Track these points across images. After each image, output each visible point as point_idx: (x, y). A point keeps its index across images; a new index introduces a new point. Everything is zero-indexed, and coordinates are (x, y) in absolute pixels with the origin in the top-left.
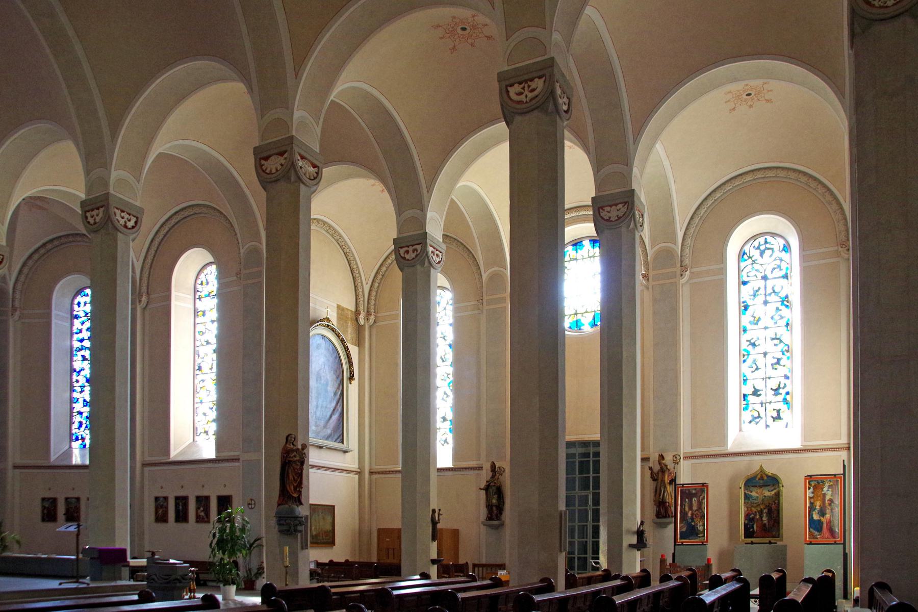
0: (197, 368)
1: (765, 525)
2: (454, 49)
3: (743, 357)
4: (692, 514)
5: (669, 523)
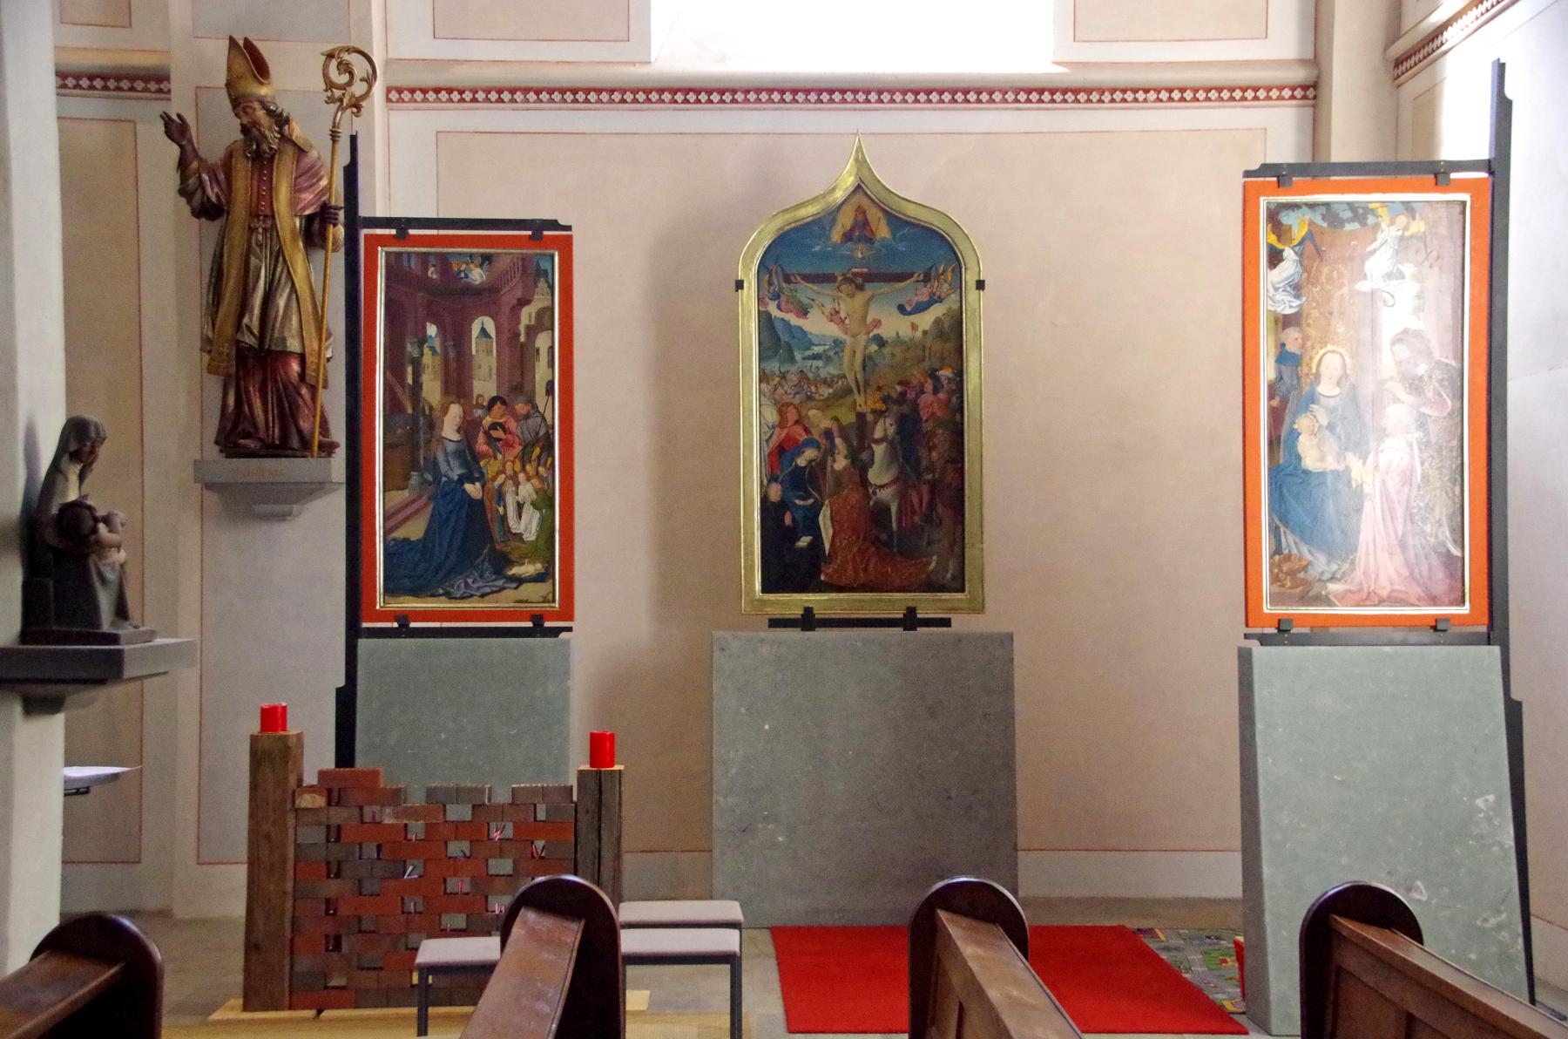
1: (882, 511)
4: (468, 428)
5: (316, 488)
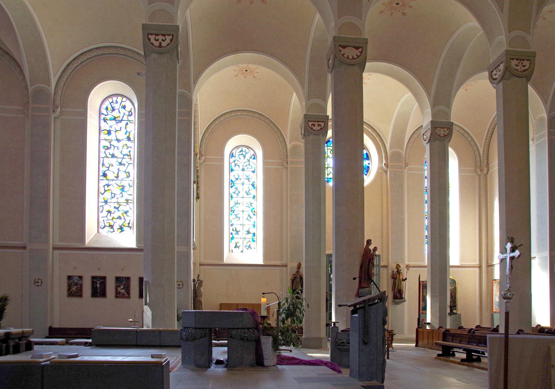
0: (101, 174)
3: (232, 211)
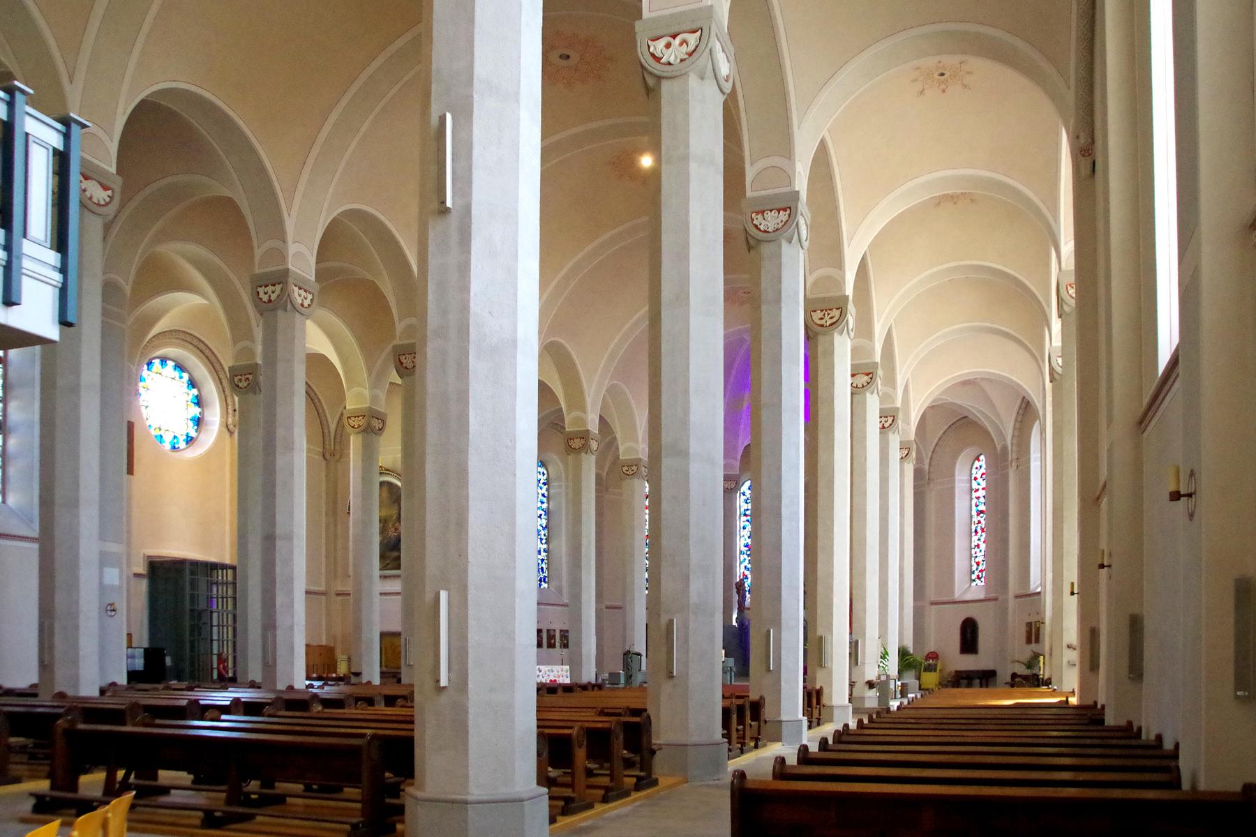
2: (922, 92)
